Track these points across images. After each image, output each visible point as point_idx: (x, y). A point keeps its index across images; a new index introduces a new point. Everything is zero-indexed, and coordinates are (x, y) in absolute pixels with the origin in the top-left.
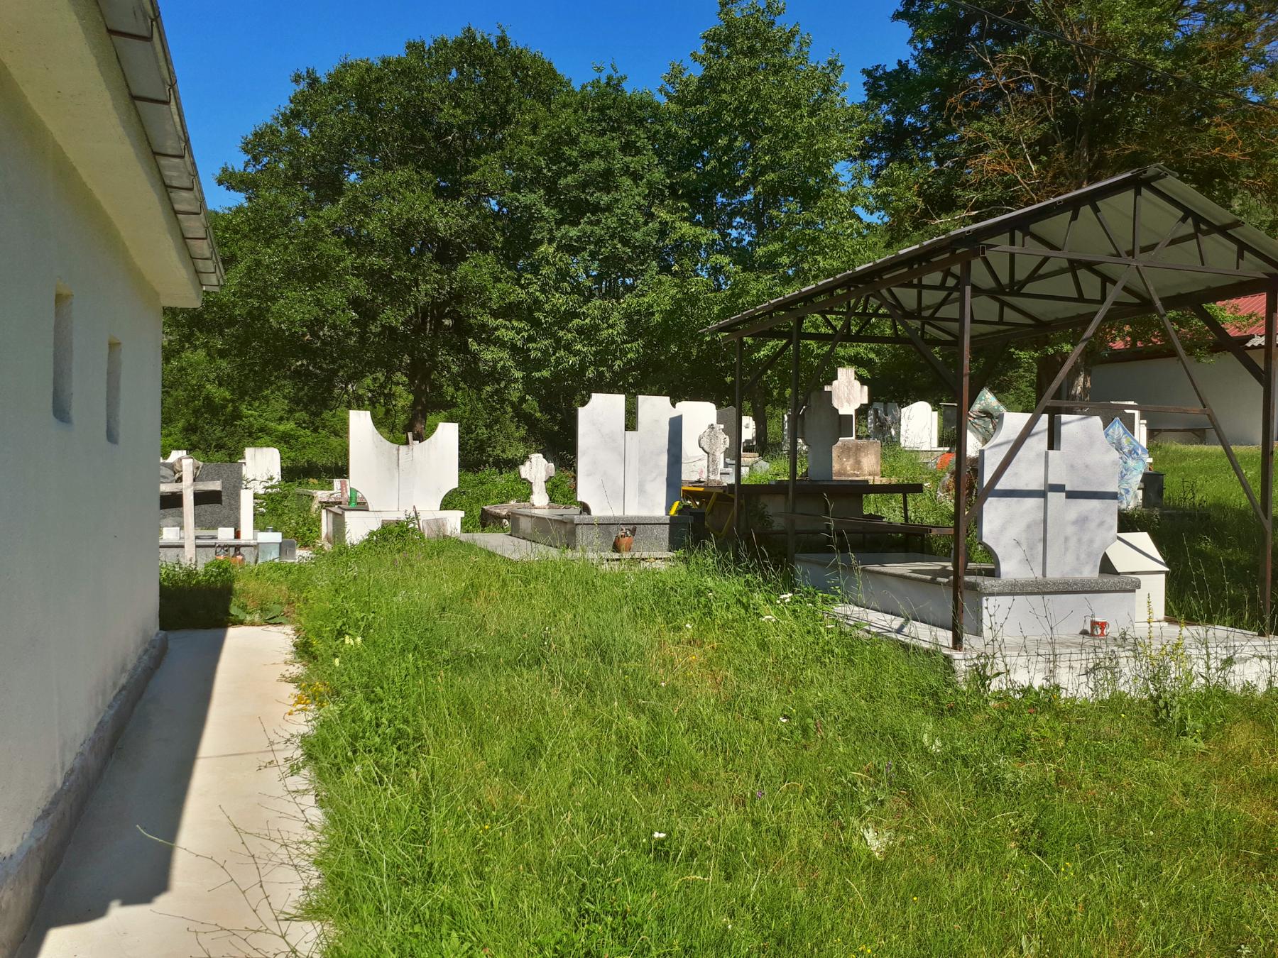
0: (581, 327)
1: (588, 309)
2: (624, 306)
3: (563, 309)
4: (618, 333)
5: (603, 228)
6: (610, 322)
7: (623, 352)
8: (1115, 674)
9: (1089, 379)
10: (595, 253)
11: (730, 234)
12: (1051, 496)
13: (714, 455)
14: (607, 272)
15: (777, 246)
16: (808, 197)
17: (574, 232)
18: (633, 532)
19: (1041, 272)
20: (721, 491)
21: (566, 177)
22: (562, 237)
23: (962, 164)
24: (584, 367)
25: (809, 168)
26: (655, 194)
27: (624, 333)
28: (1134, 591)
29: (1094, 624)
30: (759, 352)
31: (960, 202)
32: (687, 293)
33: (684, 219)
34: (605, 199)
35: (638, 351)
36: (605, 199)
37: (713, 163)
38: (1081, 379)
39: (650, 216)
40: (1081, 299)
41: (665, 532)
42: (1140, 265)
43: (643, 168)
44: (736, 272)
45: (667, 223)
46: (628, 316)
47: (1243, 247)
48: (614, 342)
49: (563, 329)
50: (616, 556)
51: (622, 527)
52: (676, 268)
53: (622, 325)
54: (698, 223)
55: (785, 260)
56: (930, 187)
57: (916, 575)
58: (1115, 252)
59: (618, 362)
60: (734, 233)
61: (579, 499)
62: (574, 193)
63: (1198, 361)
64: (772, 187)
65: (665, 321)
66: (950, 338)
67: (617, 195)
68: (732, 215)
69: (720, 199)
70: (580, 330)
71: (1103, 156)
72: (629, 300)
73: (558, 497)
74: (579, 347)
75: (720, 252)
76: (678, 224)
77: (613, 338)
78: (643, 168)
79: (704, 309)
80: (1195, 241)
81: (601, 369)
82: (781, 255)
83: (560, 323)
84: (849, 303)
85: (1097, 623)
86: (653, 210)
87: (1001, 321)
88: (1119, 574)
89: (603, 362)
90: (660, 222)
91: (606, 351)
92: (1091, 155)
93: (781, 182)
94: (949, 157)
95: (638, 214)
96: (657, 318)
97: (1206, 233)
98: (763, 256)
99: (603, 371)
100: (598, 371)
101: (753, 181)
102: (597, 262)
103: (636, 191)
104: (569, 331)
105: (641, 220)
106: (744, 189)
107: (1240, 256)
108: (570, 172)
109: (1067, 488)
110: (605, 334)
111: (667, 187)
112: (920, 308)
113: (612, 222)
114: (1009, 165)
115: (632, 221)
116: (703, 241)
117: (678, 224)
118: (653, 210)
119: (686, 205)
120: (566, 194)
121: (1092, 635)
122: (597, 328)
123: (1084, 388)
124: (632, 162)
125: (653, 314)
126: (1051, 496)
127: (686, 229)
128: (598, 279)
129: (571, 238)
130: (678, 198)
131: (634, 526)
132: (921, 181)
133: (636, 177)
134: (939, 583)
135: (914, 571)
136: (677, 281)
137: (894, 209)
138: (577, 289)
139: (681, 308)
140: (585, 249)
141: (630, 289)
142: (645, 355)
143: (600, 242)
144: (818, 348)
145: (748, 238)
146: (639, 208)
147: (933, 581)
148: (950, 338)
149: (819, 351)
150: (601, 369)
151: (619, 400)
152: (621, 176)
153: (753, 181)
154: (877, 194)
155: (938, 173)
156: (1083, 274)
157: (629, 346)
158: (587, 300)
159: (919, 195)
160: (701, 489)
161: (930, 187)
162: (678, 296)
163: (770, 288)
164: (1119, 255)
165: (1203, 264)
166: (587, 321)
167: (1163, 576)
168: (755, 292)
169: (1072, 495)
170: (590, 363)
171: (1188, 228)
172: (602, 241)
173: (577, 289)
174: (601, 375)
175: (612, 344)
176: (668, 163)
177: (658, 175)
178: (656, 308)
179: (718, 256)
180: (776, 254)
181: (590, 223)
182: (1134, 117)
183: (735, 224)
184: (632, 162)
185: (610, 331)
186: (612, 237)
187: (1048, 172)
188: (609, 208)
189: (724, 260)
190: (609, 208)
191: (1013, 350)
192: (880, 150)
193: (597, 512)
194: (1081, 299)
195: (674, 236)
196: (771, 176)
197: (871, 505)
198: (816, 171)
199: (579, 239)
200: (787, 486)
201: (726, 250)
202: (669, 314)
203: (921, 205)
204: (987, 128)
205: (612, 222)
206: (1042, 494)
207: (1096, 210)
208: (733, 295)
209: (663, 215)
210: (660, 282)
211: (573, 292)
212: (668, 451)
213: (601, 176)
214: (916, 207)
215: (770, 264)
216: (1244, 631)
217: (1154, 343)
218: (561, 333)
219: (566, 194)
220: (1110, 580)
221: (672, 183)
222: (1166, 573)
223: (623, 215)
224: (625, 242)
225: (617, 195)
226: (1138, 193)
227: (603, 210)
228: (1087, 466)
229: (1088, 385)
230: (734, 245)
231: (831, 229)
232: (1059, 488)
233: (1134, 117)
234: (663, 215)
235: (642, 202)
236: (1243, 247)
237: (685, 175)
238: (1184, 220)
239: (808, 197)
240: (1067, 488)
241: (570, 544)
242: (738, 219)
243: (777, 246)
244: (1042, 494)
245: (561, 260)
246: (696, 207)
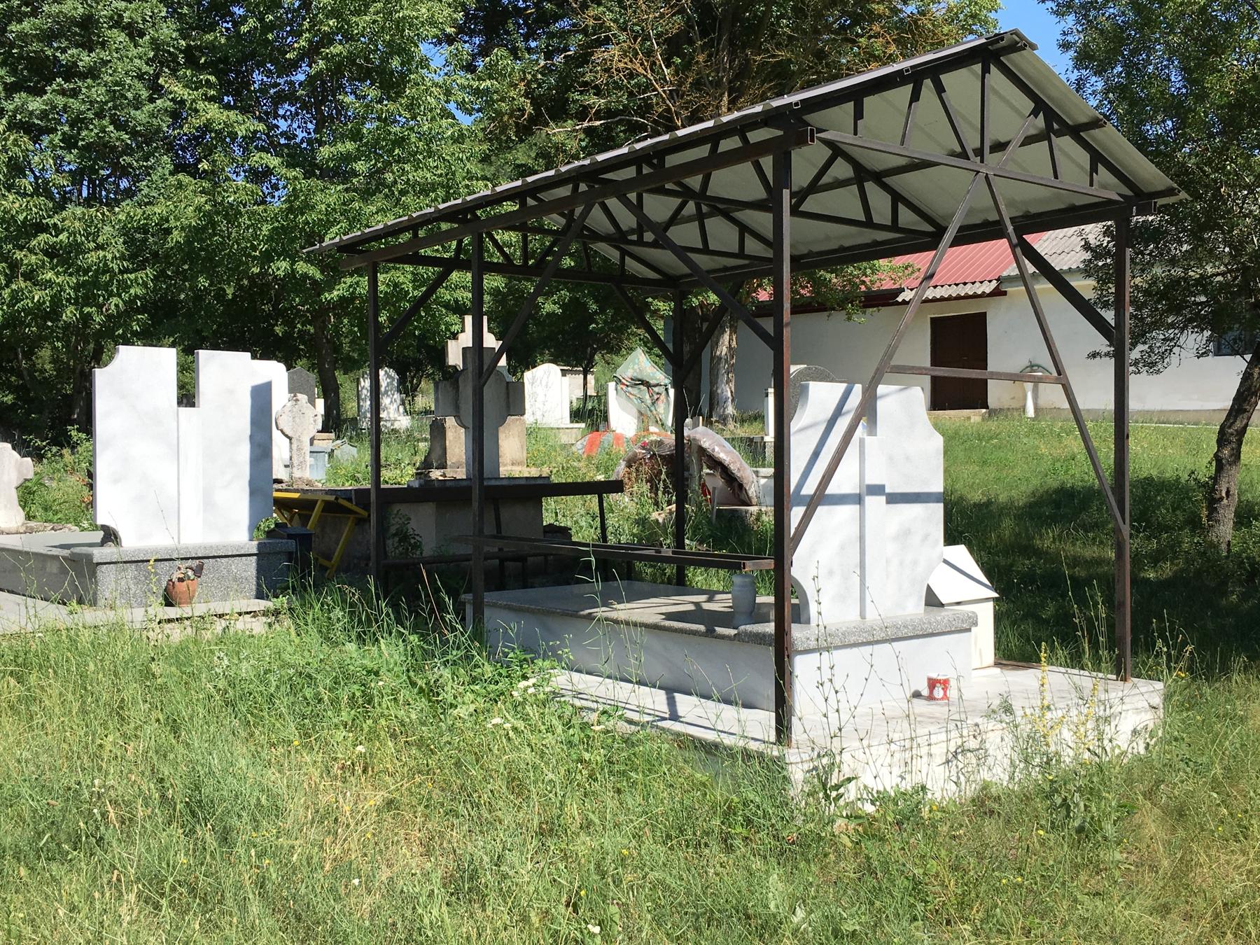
0: (53, 246)
1: (64, 220)
2: (122, 217)
3: (21, 217)
4: (114, 257)
5: (84, 102)
6: (100, 240)
7: (124, 286)
8: (982, 754)
9: (734, 337)
10: (71, 137)
11: (278, 127)
12: (870, 501)
13: (299, 440)
14: (92, 167)
15: (350, 146)
16: (392, 85)
17: (36, 104)
18: (198, 571)
19: (825, 179)
20: (332, 498)
21: (20, 21)
22: (16, 111)
23: (583, 58)
24: (57, 302)
25: (389, 44)
26: (163, 58)
27: (123, 258)
28: (969, 630)
29: (932, 684)
30: (330, 291)
31: (573, 108)
32: (222, 203)
33: (211, 99)
34: (86, 60)
35: (145, 285)
36: (86, 60)
37: (252, 22)
38: (726, 337)
39: (156, 90)
40: (869, 223)
41: (249, 568)
42: (991, 173)
43: (144, 20)
44: (296, 178)
45: (182, 102)
46: (125, 232)
47: (1097, 158)
48: (107, 270)
49: (21, 248)
50: (172, 612)
51: (178, 563)
52: (204, 165)
53: (119, 246)
54: (228, 107)
55: (361, 166)
56: (540, 86)
57: (668, 623)
58: (958, 149)
59: (114, 300)
60: (283, 125)
61: (100, 522)
62: (35, 46)
63: (849, 319)
64: (340, 64)
65: (188, 242)
66: (652, 275)
67: (104, 55)
68: (279, 99)
69: (257, 76)
70: (51, 252)
71: (747, 62)
72: (126, 210)
73: (36, 509)
74: (50, 275)
75: (263, 149)
76: (200, 105)
77: (106, 265)
78: (144, 20)
79: (248, 228)
80: (1046, 143)
81: (87, 310)
82: (356, 159)
83: (17, 238)
84: (572, 212)
85: (939, 681)
86: (161, 81)
87: (741, 254)
88: (942, 605)
89: (89, 299)
90: (172, 100)
91: (95, 283)
92: (731, 61)
93: (351, 58)
94: (559, 51)
95: (138, 85)
96: (177, 236)
97: (1059, 134)
98: (330, 159)
99: (89, 314)
100: (81, 313)
101: (311, 53)
102: (75, 151)
103: (133, 52)
104: (31, 251)
105: (145, 94)
106: (294, 65)
107: (1094, 169)
108: (26, 15)
109: (887, 490)
110: (92, 257)
111: (181, 51)
112: (700, 217)
113: (98, 93)
114: (642, 64)
115: (129, 95)
116: (241, 131)
117: (200, 105)
118: (161, 81)
119: (212, 78)
120: (21, 47)
121: (931, 698)
122: (77, 248)
123: (730, 347)
124: (127, 9)
125: (168, 232)
126: (870, 501)
127: (213, 112)
128: (76, 177)
129: (31, 113)
130: (200, 68)
131: (199, 563)
132: (529, 77)
133: (133, 32)
134: (723, 637)
135: (670, 616)
136: (206, 184)
137: (495, 111)
138: (42, 189)
139: (214, 224)
140: (54, 131)
141: (129, 193)
142: (155, 291)
143: (78, 122)
144: (414, 289)
145: (301, 135)
146: (140, 77)
147: (710, 633)
148: (652, 275)
149: (416, 293)
150: (87, 310)
151: (165, 358)
152: (110, 28)
153: (311, 53)
154: (478, 88)
155: (547, 71)
156: (870, 187)
157: (132, 276)
158: (59, 207)
159: (526, 95)
160: (296, 495)
161: (540, 86)
162: (208, 207)
163: (344, 204)
164: (964, 155)
165: (1056, 177)
166: (63, 237)
167: (991, 604)
168: (323, 207)
169: (894, 499)
170: (68, 300)
171: (1040, 122)
172: (82, 121)
173: (42, 189)
174: (86, 319)
175: (104, 272)
176: (181, 17)
177: (168, 31)
178: (172, 223)
179: (263, 155)
180: (347, 158)
181: (63, 92)
182: (778, 18)
183: (281, 112)
184: (127, 9)
185: (101, 253)
186: (100, 115)
187: (687, 77)
188: (92, 73)
189: (273, 161)
190: (92, 73)
191: (650, 300)
192: (472, 33)
193: (132, 541)
194: (869, 223)
195: (197, 122)
196: (336, 49)
197: (554, 511)
198: (402, 51)
199: (44, 115)
200: (469, 489)
201: (272, 146)
202: (195, 233)
203: (529, 109)
204: (609, 16)
205: (98, 93)
206: (858, 499)
207: (940, 89)
208: (290, 210)
209: (178, 90)
210: (180, 186)
211: (36, 192)
212: (251, 437)
213: (78, 25)
214: (523, 111)
215: (338, 172)
216: (1069, 670)
217: (802, 296)
218: (19, 255)
219: (21, 47)
220: (940, 616)
221: (188, 46)
222: (995, 600)
223: (117, 84)
224: (120, 126)
225: (104, 55)
226: (986, 70)
227: (83, 76)
228: (907, 458)
229: (734, 344)
230: (283, 141)
231: (425, 128)
232: (876, 490)
233: (778, 18)
234: (178, 90)
235: (145, 68)
236: (1097, 158)
237: (210, 37)
238: (1035, 113)
239: (392, 85)
240: (887, 490)
241: (86, 598)
242: (286, 106)
243: (350, 146)
244: (858, 499)
245: (15, 143)
246: (226, 86)
